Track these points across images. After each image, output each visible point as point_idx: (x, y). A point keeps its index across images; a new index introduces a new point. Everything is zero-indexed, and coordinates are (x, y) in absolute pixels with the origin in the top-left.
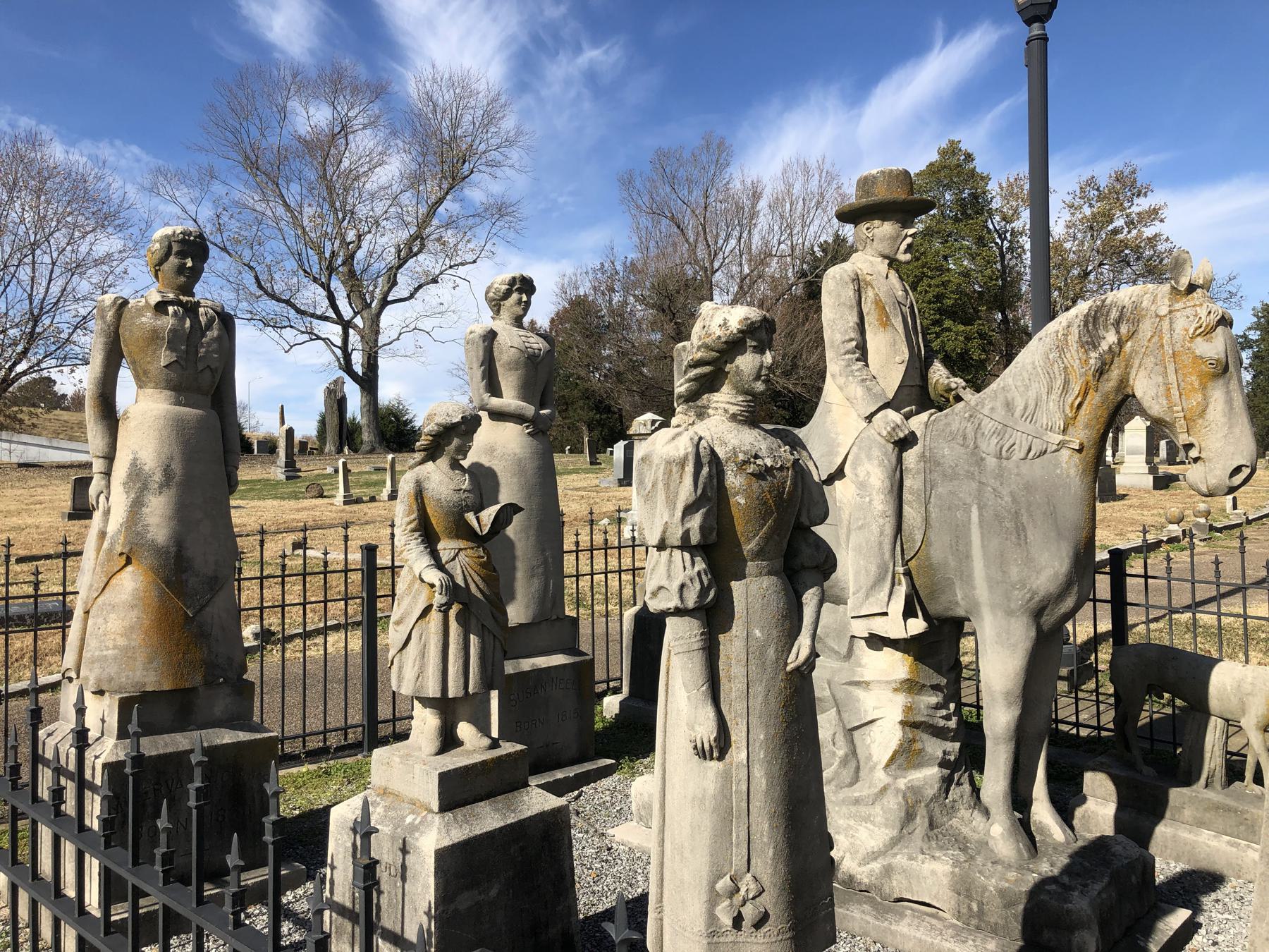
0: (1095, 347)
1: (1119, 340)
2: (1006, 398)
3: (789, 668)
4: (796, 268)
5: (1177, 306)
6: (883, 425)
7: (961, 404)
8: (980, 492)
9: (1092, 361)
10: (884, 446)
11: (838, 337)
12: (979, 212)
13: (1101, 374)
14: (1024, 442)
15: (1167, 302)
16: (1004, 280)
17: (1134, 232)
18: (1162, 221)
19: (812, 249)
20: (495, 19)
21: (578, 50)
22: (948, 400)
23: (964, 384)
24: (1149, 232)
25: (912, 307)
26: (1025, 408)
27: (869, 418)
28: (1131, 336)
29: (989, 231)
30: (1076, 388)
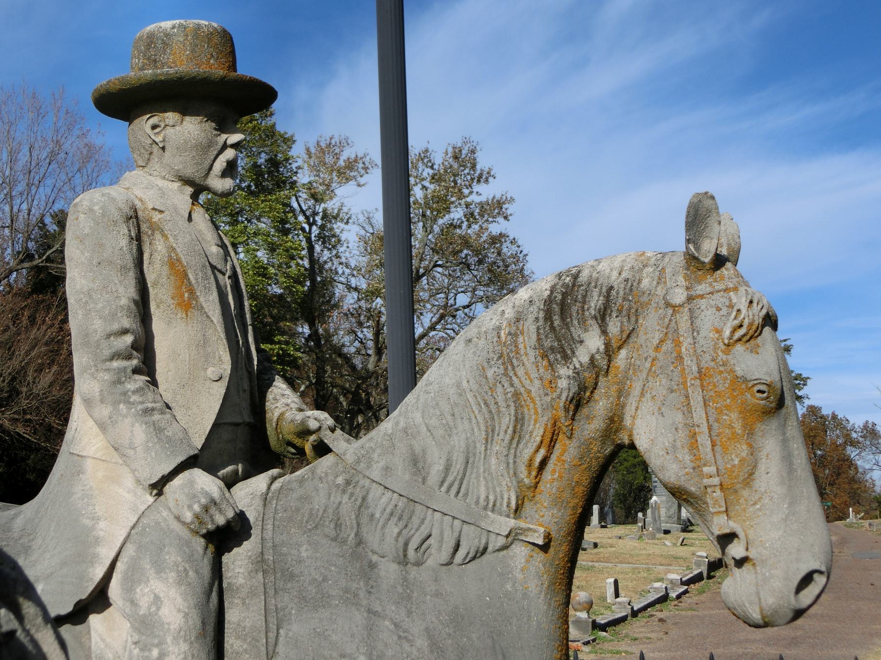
0: (566, 358)
1: (607, 345)
2: (411, 447)
4: (18, 247)
5: (701, 289)
6: (182, 498)
7: (328, 460)
8: (370, 630)
9: (563, 383)
10: (188, 543)
11: (98, 326)
12: (280, 184)
13: (578, 406)
14: (447, 533)
15: (681, 280)
16: (313, 281)
17: (476, 227)
18: (506, 218)
19: (42, 221)
22: (301, 452)
23: (331, 422)
24: (495, 229)
25: (234, 277)
26: (447, 469)
27: (159, 487)
28: (627, 339)
29: (293, 211)
30: (536, 431)
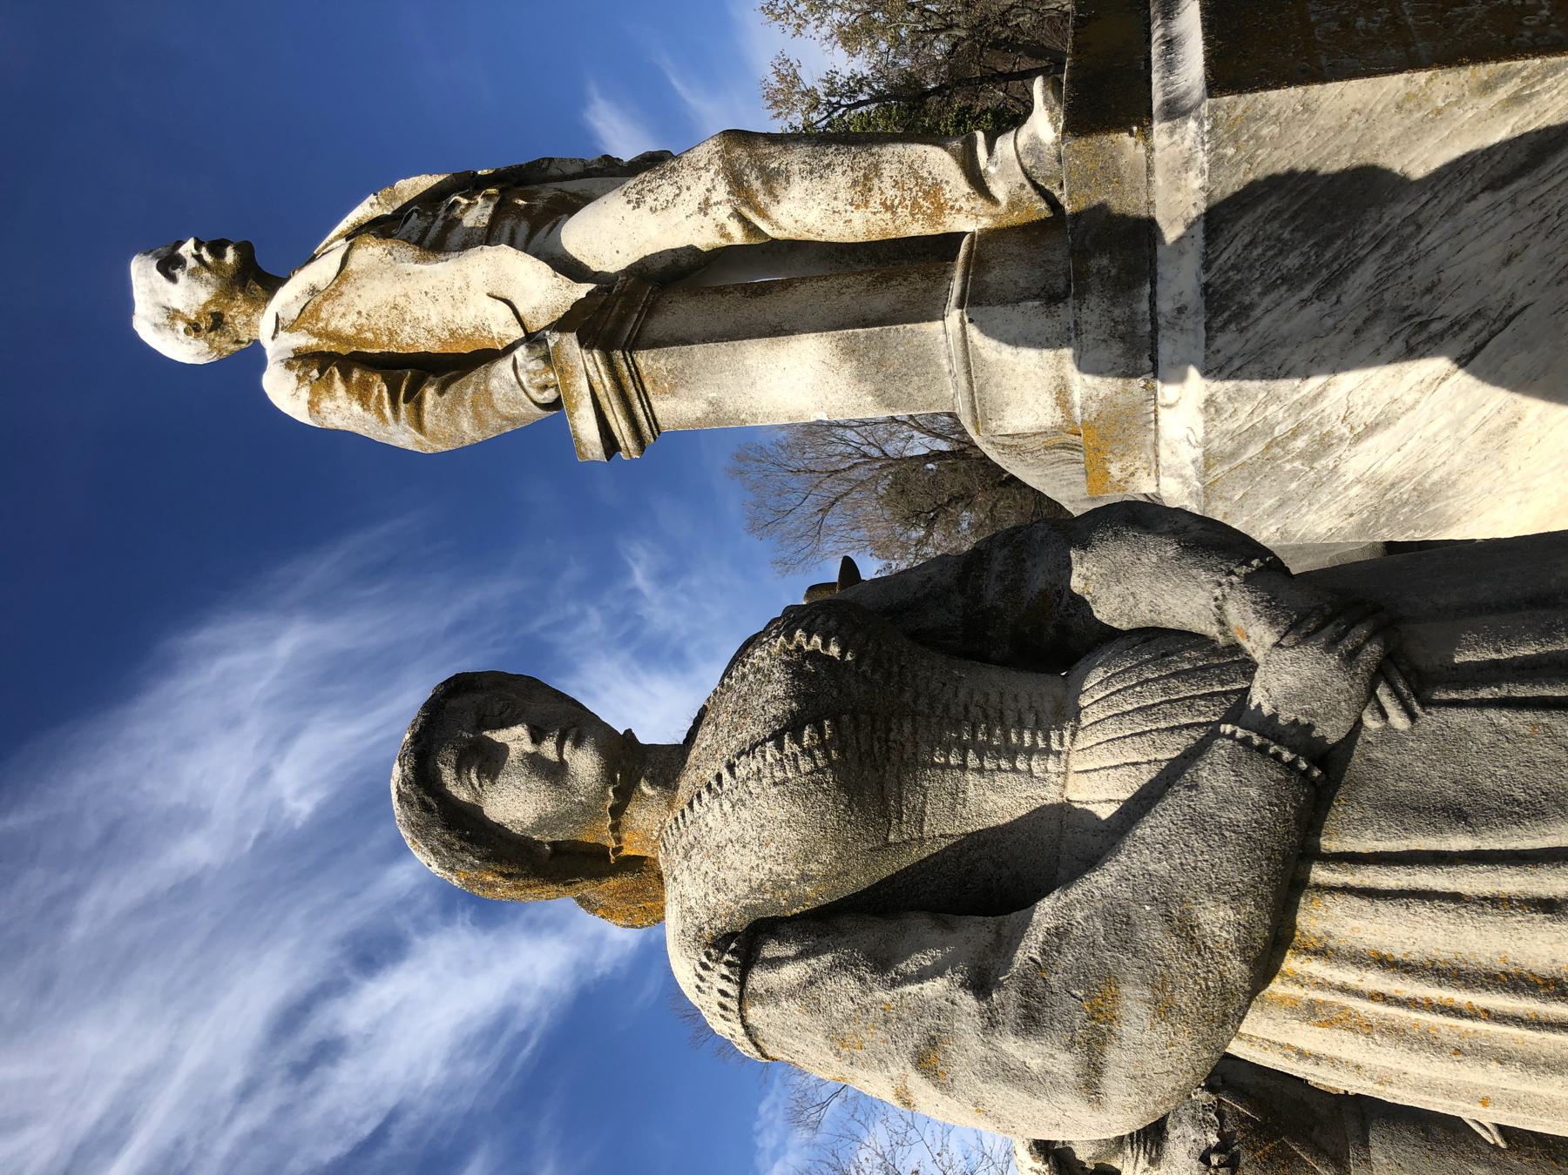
3: (1503, 1145)
20: (606, 688)
21: (635, 592)
